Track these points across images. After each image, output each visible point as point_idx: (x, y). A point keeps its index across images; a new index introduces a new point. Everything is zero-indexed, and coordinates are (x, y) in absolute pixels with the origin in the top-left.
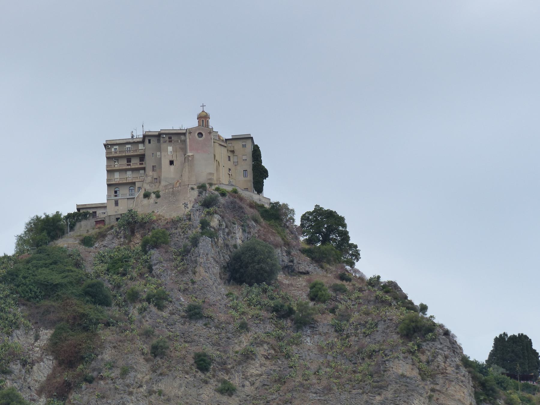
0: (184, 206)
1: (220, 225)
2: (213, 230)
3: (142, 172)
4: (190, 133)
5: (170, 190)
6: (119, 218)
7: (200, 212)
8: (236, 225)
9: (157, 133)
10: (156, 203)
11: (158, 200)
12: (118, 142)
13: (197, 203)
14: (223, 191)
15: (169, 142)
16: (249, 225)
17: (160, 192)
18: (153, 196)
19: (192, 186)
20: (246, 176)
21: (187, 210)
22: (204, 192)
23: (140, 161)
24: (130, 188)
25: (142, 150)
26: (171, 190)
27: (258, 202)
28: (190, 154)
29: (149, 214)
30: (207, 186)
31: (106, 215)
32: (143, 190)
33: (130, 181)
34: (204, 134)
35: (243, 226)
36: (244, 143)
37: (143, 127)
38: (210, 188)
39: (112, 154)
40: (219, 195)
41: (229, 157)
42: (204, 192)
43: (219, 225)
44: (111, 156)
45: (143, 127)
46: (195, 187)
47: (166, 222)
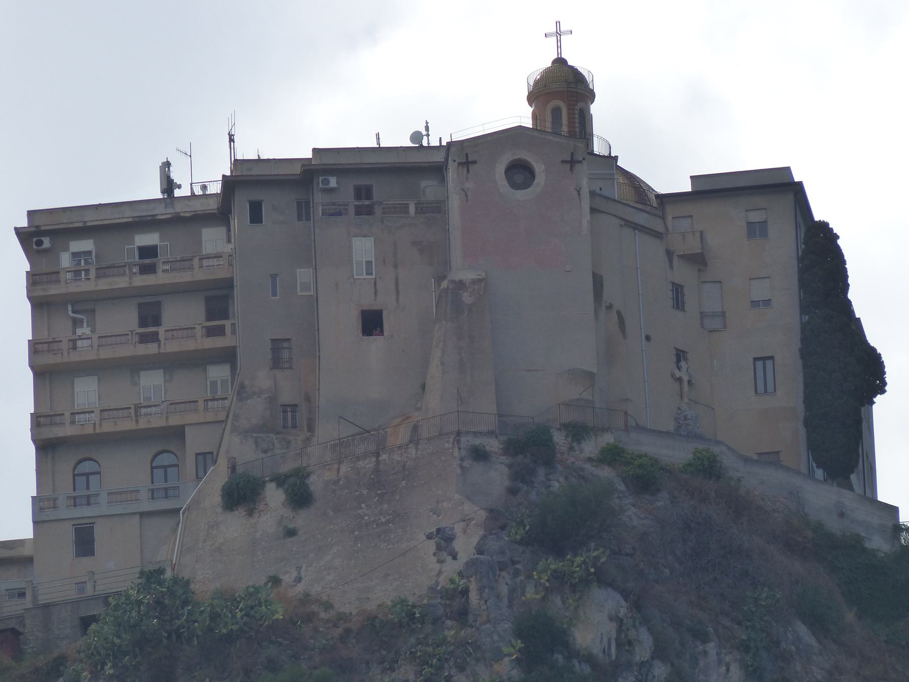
0: (431, 546)
1: (625, 644)
2: (587, 669)
3: (219, 373)
4: (467, 164)
5: (361, 464)
6: (94, 619)
7: (516, 573)
8: (711, 647)
9: (297, 170)
10: (291, 533)
11: (301, 520)
12: (92, 219)
13: (503, 528)
14: (640, 466)
15: (359, 211)
16: (777, 643)
17: (313, 478)
18: (274, 496)
19: (477, 441)
20: (770, 388)
21: (451, 568)
22: (541, 471)
23: (210, 316)
24: (158, 461)
25: (218, 256)
26: (368, 464)
27: (834, 525)
28: (468, 276)
29: (253, 593)
30: (559, 439)
31: (28, 602)
32: (222, 464)
33: (154, 424)
34: (539, 168)
35: (745, 647)
36: (755, 217)
37: (231, 140)
38: (571, 448)
39: (58, 281)
40: (622, 487)
41: (678, 290)
42: (541, 471)
43: (619, 645)
44: (54, 290)
45: (231, 140)
46: (493, 445)
47: (340, 630)
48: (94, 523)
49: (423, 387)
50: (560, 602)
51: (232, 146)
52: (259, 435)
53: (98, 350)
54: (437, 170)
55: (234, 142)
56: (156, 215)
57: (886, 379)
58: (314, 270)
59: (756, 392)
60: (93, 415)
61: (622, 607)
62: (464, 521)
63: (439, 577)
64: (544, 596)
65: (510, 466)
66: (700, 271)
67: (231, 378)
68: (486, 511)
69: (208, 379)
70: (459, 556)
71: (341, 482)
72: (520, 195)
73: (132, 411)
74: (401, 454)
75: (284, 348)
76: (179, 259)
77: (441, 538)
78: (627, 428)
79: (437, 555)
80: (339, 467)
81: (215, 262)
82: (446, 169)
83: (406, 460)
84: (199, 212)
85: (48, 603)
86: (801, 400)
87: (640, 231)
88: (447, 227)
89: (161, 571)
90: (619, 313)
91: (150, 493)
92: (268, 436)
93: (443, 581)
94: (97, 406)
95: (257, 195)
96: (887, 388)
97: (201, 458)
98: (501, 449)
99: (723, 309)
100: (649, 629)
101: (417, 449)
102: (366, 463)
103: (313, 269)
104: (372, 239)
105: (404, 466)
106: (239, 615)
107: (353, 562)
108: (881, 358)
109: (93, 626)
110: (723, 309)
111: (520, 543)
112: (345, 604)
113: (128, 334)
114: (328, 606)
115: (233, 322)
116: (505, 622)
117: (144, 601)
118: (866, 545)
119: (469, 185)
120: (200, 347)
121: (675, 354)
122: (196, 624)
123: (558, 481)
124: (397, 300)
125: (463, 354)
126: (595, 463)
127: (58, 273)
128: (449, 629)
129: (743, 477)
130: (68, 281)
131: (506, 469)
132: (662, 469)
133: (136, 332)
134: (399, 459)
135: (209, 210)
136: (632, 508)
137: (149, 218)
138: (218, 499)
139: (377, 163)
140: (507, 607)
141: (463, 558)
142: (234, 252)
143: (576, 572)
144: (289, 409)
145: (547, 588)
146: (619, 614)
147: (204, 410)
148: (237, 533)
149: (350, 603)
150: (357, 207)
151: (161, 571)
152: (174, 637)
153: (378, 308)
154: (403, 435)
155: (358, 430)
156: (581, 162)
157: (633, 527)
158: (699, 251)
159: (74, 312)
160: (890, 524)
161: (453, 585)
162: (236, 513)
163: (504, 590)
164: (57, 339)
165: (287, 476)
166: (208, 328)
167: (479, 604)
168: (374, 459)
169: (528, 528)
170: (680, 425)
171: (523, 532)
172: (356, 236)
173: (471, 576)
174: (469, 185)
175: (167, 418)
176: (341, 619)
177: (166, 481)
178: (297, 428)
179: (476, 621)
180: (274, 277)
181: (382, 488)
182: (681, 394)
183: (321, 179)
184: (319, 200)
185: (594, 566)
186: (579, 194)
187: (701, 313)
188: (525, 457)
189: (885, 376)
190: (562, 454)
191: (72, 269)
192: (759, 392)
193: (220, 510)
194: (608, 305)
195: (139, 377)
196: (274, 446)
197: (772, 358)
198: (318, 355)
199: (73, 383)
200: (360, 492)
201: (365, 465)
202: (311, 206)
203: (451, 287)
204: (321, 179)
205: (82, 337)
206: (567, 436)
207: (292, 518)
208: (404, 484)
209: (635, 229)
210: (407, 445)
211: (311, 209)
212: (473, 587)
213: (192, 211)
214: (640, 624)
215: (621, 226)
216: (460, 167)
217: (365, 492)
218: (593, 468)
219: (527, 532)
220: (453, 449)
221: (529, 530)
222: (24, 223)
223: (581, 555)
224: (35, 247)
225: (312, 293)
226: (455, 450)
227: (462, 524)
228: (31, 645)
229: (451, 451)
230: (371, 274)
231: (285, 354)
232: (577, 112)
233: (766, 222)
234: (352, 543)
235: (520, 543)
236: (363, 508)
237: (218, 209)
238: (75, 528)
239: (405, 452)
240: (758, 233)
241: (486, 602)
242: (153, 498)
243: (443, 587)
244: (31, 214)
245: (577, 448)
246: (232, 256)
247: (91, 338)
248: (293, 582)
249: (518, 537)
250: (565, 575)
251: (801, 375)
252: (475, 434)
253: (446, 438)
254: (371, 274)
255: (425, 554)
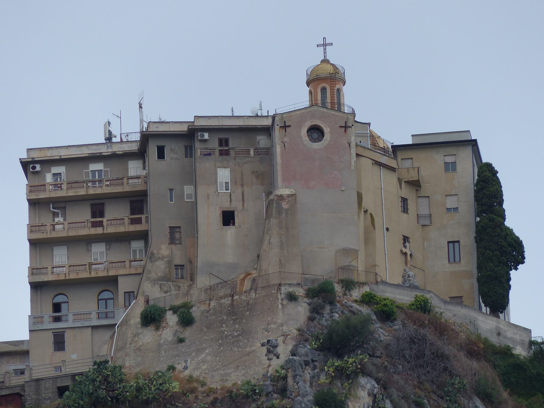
0: (264, 350)
3: (137, 245)
4: (285, 127)
7: (315, 368)
9: (185, 128)
10: (181, 341)
11: (188, 333)
12: (64, 154)
14: (385, 305)
15: (222, 153)
17: (194, 309)
18: (172, 319)
19: (291, 290)
20: (457, 259)
21: (276, 363)
22: (328, 308)
25: (138, 177)
26: (227, 301)
27: (494, 340)
28: (285, 192)
30: (338, 288)
36: (449, 159)
37: (141, 107)
38: (345, 294)
39: (45, 190)
40: (374, 317)
41: (404, 201)
42: (328, 308)
44: (42, 196)
45: (141, 107)
46: (300, 292)
48: (65, 332)
49: (258, 256)
50: (340, 385)
51: (141, 111)
52: (162, 283)
53: (68, 231)
54: (267, 131)
55: (142, 108)
56: (102, 153)
57: (525, 255)
58: (195, 187)
59: (449, 261)
60: (65, 268)
61: (375, 388)
62: (283, 336)
63: (269, 368)
64: (331, 381)
65: (309, 304)
66: (417, 190)
67: (145, 248)
68: (296, 330)
69: (131, 249)
70: (280, 357)
71: (211, 312)
72: (316, 146)
73: (87, 266)
74: (247, 295)
75: (177, 232)
76: (115, 178)
77: (270, 346)
78: (377, 283)
79: (267, 355)
80: (210, 302)
81: (136, 181)
82: (272, 130)
83: (249, 299)
84: (127, 151)
85: (39, 378)
86: (475, 266)
87: (383, 166)
88: (272, 163)
89: (107, 362)
90: (371, 215)
91: (97, 314)
92: (167, 283)
93: (271, 371)
94: (67, 263)
95: (161, 143)
96: (525, 260)
97: (127, 295)
98: (305, 294)
99: (430, 213)
100: (391, 401)
101: (256, 293)
102: (225, 300)
103: (194, 186)
104: (229, 169)
105: (248, 304)
106: (153, 389)
107: (218, 358)
108: (522, 243)
109: (67, 393)
110: (430, 213)
111: (316, 349)
112: (213, 383)
113: (85, 222)
114: (203, 384)
115: (147, 216)
116: (309, 396)
117: (97, 379)
118: (513, 352)
119: (286, 139)
120: (127, 230)
121: (403, 238)
122: (128, 394)
123: (337, 313)
124: (243, 205)
125: (283, 238)
126: (358, 303)
127: (45, 185)
128: (276, 399)
129: (443, 312)
130: (50, 190)
131: (307, 306)
132: (397, 307)
133: (90, 220)
134: (245, 299)
135: (133, 150)
136: (380, 329)
137: (98, 154)
138: (138, 320)
139: (232, 125)
140: (309, 387)
141: (283, 358)
142: (148, 175)
143: (350, 367)
144: (179, 268)
145: (332, 376)
146: (374, 392)
147: (129, 267)
148: (150, 340)
149: (216, 382)
150: (220, 150)
151: (107, 362)
152: (114, 400)
153: (232, 210)
154: (247, 285)
155: (218, 281)
156: (351, 127)
157: (381, 341)
158: (417, 179)
159: (53, 208)
160: (527, 340)
161: (278, 374)
162: (149, 328)
163: (308, 377)
164: (44, 224)
165: (179, 307)
166: (131, 219)
167: (293, 385)
168: (230, 298)
169: (321, 340)
170: (405, 280)
171: (318, 343)
172: (219, 168)
173: (289, 369)
174: (286, 139)
175: (108, 271)
176: (211, 391)
177: (106, 308)
178: (184, 279)
179: (291, 395)
180: (171, 190)
181: (235, 315)
182: (406, 262)
183: (199, 134)
184: (198, 147)
185: (360, 364)
186: (350, 146)
187: (418, 215)
188: (319, 299)
189: (525, 253)
190: (340, 297)
191: (53, 183)
192: (450, 262)
193: (140, 326)
194: (365, 210)
195: (91, 246)
196: (171, 289)
197: (458, 242)
198: (196, 236)
199: (53, 250)
200: (222, 317)
201: (225, 302)
202: (193, 149)
203: (276, 198)
204: (199, 134)
205: (58, 223)
206: (343, 287)
207: (182, 332)
208: (248, 314)
209: (380, 166)
210: (250, 291)
211: (193, 151)
212: (290, 375)
213: (123, 151)
214: (386, 398)
215: (373, 164)
216: (281, 129)
217: (225, 318)
218: (358, 306)
219: (321, 343)
220: (277, 294)
221: (322, 343)
222: (24, 156)
223: (353, 358)
224: (31, 170)
225: (193, 200)
226: (278, 295)
227: (282, 338)
228: (29, 403)
229: (276, 294)
230: (228, 190)
231: (177, 236)
232: (335, 91)
233: (455, 162)
234: (218, 347)
235: (316, 349)
236: (224, 327)
237: (138, 149)
238: (53, 334)
239: (249, 295)
240: (451, 170)
241: (297, 384)
242: (99, 318)
243: (271, 375)
244: (29, 150)
245: (348, 294)
246: (146, 177)
247: (64, 224)
248: (183, 369)
249: (316, 346)
250: (343, 369)
251: (476, 252)
252: (290, 285)
253: (273, 287)
254: (228, 190)
255: (261, 355)
